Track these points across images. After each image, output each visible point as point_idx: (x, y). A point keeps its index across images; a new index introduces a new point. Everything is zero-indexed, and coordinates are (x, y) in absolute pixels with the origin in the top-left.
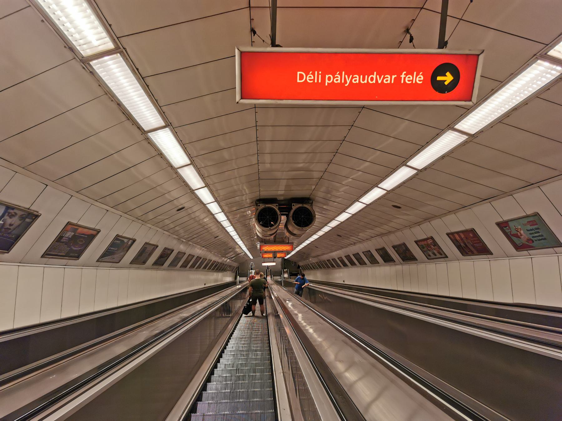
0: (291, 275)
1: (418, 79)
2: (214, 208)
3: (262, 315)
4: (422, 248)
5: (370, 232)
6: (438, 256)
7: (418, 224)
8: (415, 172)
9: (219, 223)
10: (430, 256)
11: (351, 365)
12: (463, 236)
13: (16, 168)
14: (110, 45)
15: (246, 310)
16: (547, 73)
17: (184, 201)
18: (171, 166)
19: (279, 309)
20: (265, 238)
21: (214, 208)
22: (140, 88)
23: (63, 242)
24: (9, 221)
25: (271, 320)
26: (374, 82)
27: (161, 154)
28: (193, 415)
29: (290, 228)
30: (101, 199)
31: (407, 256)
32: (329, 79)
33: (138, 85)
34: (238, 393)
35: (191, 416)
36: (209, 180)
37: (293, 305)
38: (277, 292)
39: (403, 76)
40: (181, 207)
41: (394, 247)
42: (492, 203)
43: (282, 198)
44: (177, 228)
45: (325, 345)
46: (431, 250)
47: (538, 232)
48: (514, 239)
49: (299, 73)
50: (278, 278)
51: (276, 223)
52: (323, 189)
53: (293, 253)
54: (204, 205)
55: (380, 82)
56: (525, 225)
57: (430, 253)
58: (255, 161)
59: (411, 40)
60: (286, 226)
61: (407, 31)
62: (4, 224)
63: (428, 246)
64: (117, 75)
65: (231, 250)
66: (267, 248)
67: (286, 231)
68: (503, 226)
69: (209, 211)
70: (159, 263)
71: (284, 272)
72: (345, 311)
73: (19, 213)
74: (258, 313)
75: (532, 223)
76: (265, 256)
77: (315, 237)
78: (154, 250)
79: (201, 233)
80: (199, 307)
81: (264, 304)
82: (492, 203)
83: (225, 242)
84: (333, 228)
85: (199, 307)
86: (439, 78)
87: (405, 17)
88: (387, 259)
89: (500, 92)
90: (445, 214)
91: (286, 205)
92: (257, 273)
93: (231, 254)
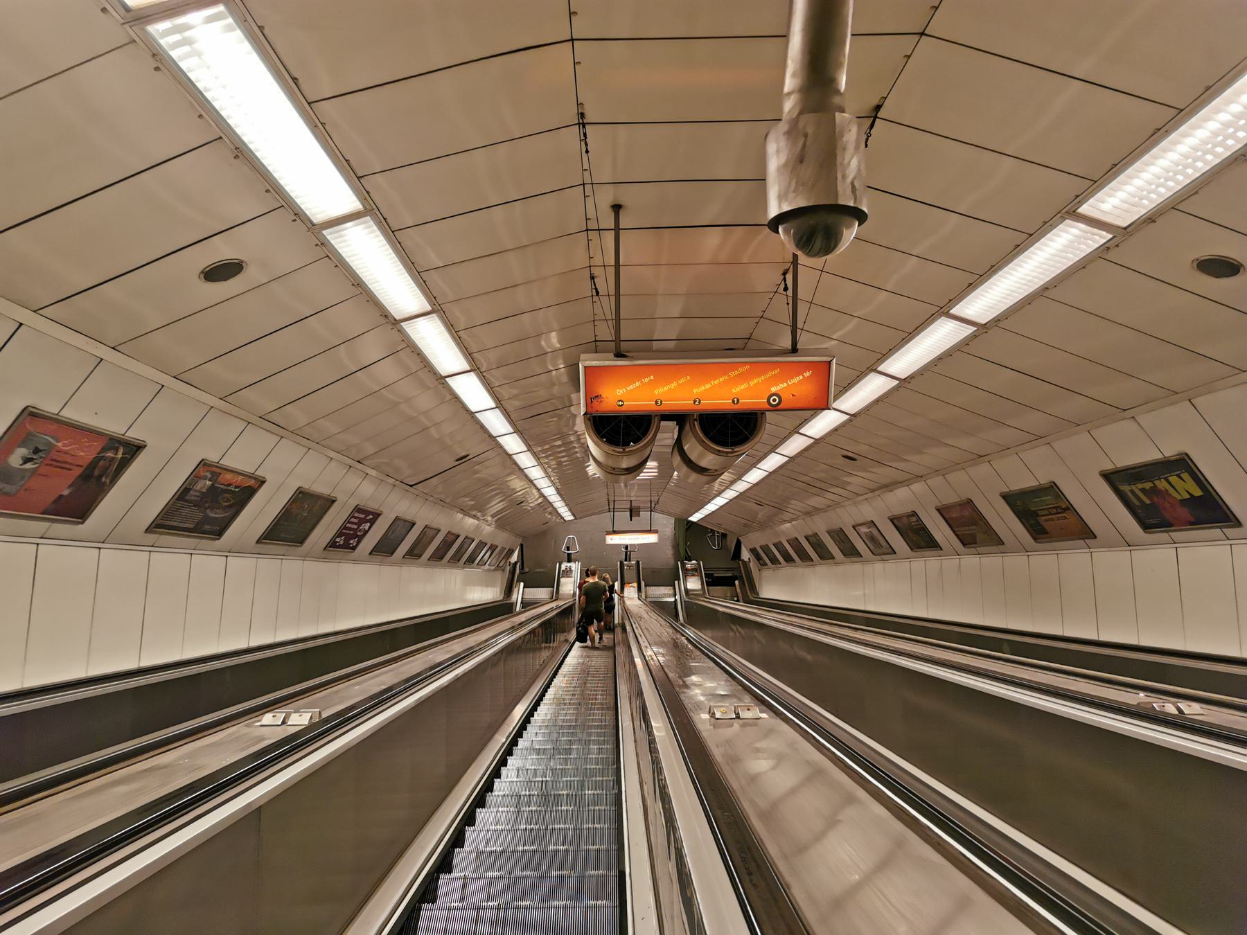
0: (712, 581)
8: (896, 382)
13: (332, 454)
16: (1086, 239)
50: (663, 593)
64: (434, 341)
71: (687, 573)
72: (828, 678)
93: (496, 505)
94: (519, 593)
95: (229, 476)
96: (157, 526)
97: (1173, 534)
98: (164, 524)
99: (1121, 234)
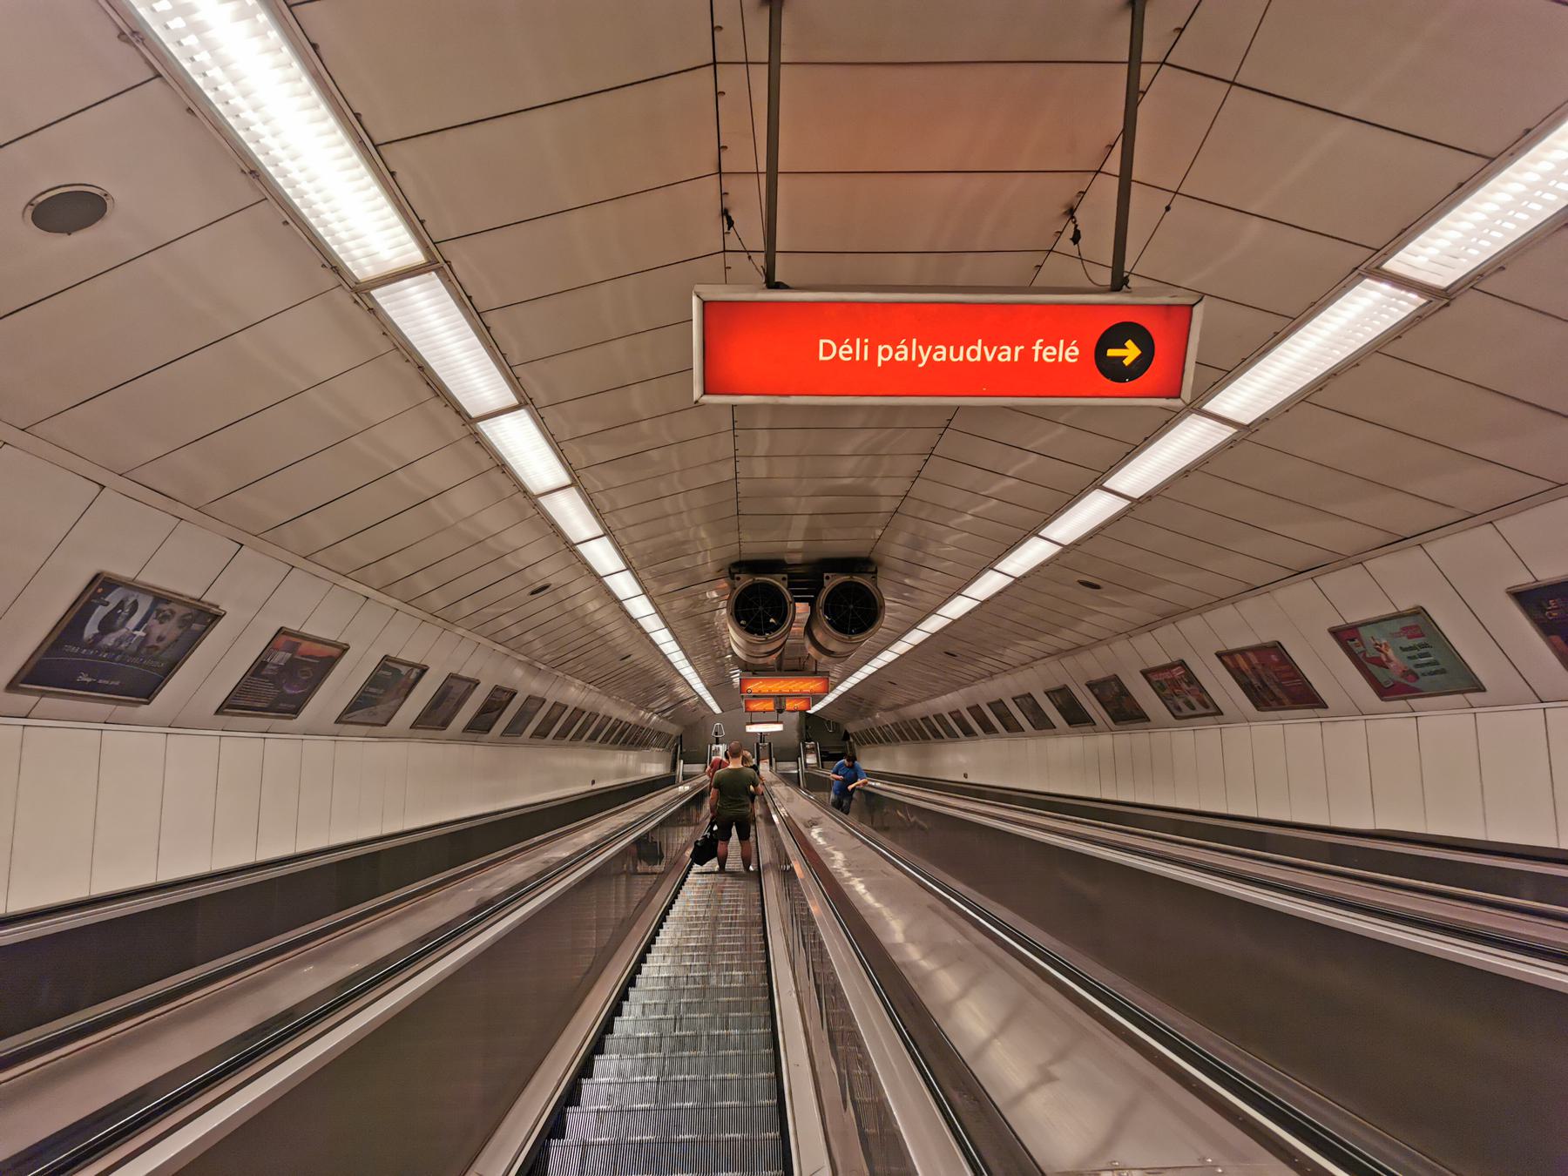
0: (826, 757)
1: (1067, 353)
2: (624, 585)
3: (747, 868)
4: (1159, 689)
5: (1027, 647)
6: (1200, 709)
7: (1148, 627)
8: (1125, 503)
9: (634, 621)
10: (1179, 709)
11: (859, 871)
12: (1254, 660)
14: (417, 256)
15: (703, 852)
16: (1390, 305)
17: (548, 571)
18: (525, 491)
19: (791, 848)
20: (753, 661)
21: (624, 585)
22: (471, 332)
23: (266, 677)
24: (158, 629)
25: (771, 883)
26: (978, 358)
27: (502, 466)
28: (554, 1142)
29: (819, 636)
30: (357, 572)
31: (1125, 712)
32: (885, 353)
33: (468, 327)
34: (680, 1086)
35: (548, 1146)
36: (612, 521)
37: (848, 864)
38: (789, 803)
39: (1037, 348)
40: (539, 585)
41: (1090, 686)
42: (1498, 524)
43: (798, 558)
44: (528, 637)
45: (886, 912)
46: (1181, 693)
47: (1426, 655)
48: (1373, 668)
49: (822, 342)
50: (789, 767)
51: (782, 620)
52: (903, 537)
53: (830, 698)
54: (599, 578)
55: (989, 359)
56: (1395, 635)
57: (1180, 703)
58: (730, 475)
59: (1076, 238)
60: (808, 630)
61: (1071, 212)
62: (145, 639)
63: (1175, 683)
64: (431, 319)
65: (661, 690)
66: (758, 686)
67: (808, 643)
68: (1345, 636)
69: (609, 592)
70: (480, 725)
71: (806, 751)
72: (964, 852)
73: (180, 611)
74: (734, 863)
75: (1411, 632)
76: (755, 706)
77: (887, 657)
78: (469, 691)
79: (587, 648)
80: (588, 837)
81: (752, 839)
82: (1498, 524)
83: (645, 672)
84: (933, 635)
85: (588, 837)
86: (1111, 353)
87: (1065, 189)
88: (1076, 717)
89: (1294, 338)
90: (1211, 606)
91: (808, 577)
92: (732, 753)
94: (681, 767)
95: (305, 645)
96: (228, 707)
97: (1412, 702)
98: (240, 703)
99: (1439, 298)
